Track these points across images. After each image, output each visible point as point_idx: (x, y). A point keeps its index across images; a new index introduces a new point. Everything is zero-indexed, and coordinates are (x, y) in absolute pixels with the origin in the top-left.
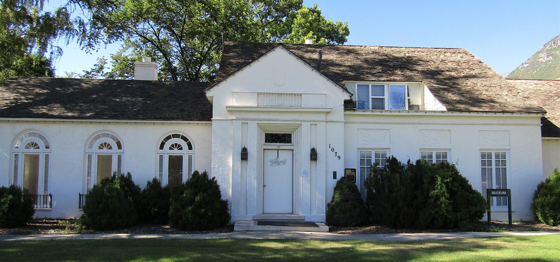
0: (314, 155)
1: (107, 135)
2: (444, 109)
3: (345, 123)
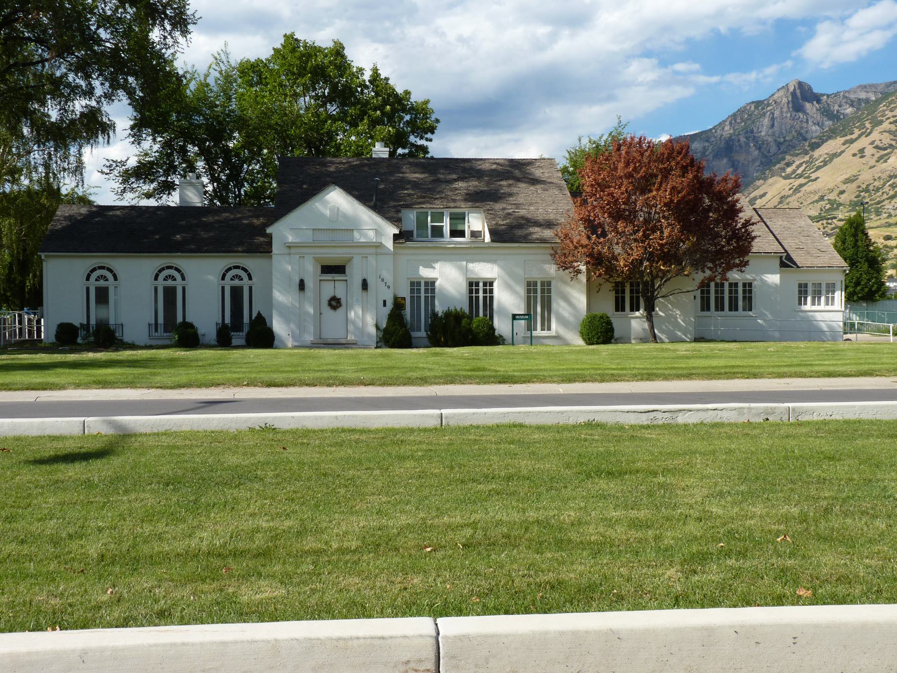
0: (365, 285)
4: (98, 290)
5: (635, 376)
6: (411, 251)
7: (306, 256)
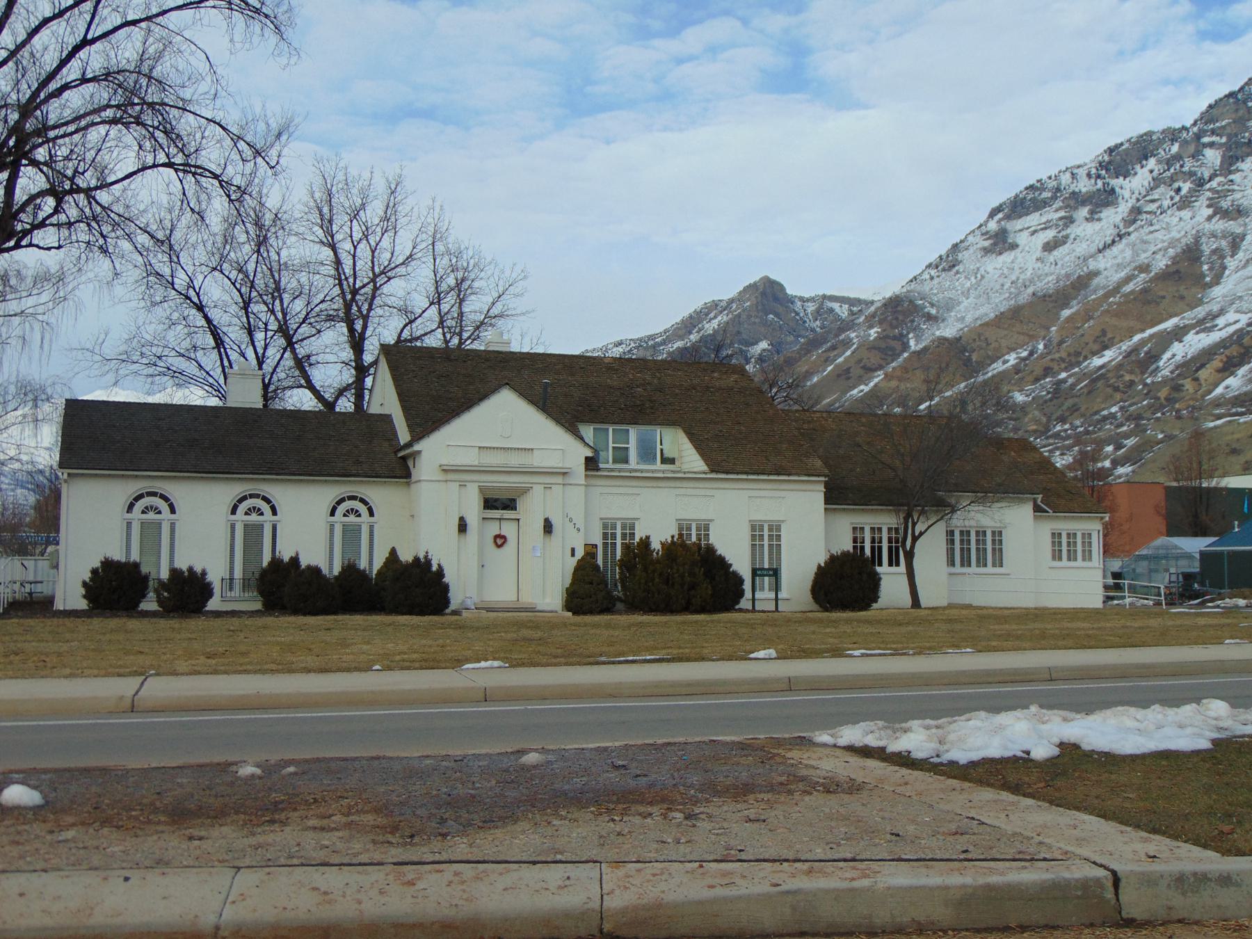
0: (548, 527)
1: (257, 496)
2: (705, 468)
3: (586, 486)
4: (346, 528)
5: (827, 651)
6: (609, 482)
7: (553, 486)
